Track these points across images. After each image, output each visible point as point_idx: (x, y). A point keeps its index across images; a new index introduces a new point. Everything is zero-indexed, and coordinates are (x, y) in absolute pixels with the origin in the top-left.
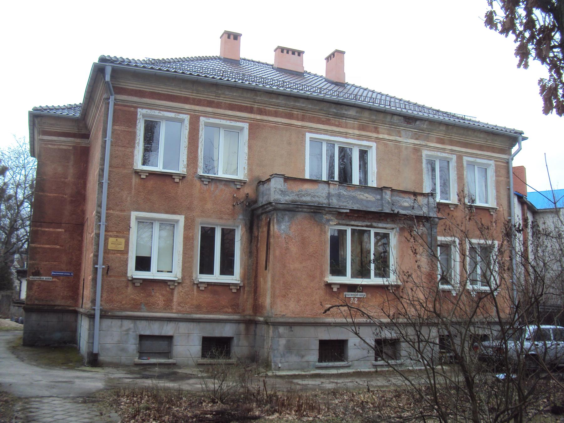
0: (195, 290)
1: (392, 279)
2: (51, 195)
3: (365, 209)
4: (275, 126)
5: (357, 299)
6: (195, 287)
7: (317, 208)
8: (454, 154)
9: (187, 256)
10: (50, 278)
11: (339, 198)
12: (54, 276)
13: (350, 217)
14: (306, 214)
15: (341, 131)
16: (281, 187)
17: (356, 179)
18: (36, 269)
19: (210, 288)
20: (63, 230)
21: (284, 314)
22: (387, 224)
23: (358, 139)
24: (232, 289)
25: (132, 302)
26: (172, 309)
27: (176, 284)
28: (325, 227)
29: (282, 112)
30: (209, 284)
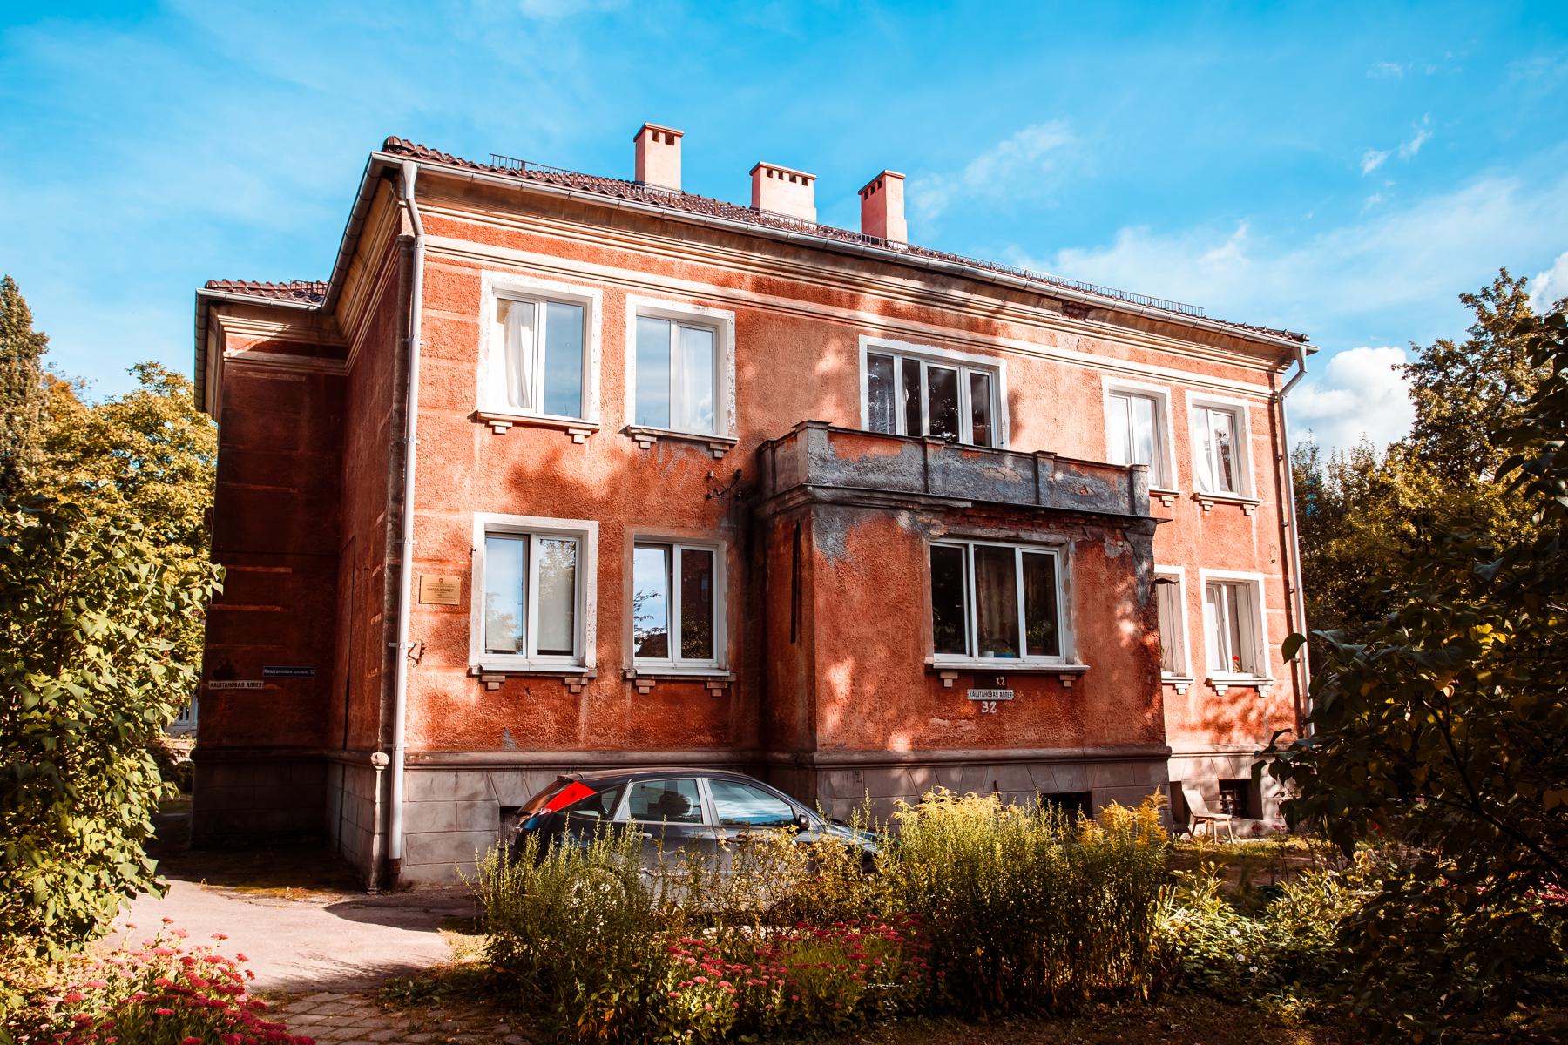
0: (629, 695)
1: (1067, 657)
2: (258, 487)
3: (1001, 500)
4: (793, 318)
5: (995, 704)
6: (629, 686)
7: (904, 498)
8: (1166, 385)
9: (607, 614)
10: (258, 684)
11: (948, 475)
12: (268, 679)
13: (971, 520)
14: (879, 511)
15: (933, 332)
16: (823, 452)
17: (966, 436)
18: (224, 663)
19: (661, 687)
20: (289, 570)
21: (840, 741)
22: (1050, 533)
23: (969, 351)
24: (711, 689)
25: (482, 728)
26: (576, 741)
27: (584, 682)
28: (921, 541)
29: (807, 287)
30: (660, 679)
